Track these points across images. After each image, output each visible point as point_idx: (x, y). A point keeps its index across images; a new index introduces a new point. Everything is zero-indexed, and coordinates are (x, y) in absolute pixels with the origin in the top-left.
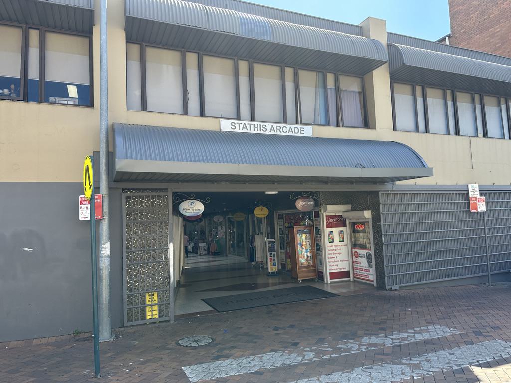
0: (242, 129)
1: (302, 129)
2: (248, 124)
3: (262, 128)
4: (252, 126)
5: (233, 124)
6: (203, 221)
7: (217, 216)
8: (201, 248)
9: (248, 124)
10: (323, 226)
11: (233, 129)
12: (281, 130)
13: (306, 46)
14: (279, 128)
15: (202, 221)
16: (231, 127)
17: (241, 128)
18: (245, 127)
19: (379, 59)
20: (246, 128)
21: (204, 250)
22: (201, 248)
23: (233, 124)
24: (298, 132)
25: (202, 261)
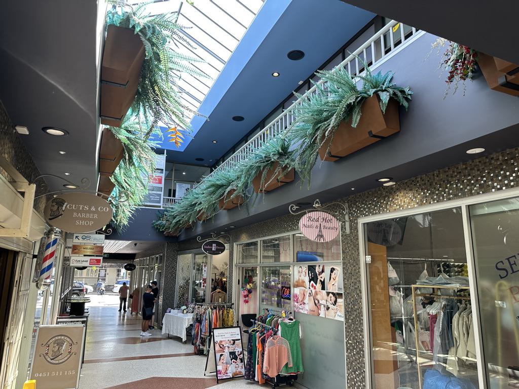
6: (226, 253)
7: (314, 215)
8: (222, 348)
15: (223, 251)
21: (233, 355)
22: (222, 348)
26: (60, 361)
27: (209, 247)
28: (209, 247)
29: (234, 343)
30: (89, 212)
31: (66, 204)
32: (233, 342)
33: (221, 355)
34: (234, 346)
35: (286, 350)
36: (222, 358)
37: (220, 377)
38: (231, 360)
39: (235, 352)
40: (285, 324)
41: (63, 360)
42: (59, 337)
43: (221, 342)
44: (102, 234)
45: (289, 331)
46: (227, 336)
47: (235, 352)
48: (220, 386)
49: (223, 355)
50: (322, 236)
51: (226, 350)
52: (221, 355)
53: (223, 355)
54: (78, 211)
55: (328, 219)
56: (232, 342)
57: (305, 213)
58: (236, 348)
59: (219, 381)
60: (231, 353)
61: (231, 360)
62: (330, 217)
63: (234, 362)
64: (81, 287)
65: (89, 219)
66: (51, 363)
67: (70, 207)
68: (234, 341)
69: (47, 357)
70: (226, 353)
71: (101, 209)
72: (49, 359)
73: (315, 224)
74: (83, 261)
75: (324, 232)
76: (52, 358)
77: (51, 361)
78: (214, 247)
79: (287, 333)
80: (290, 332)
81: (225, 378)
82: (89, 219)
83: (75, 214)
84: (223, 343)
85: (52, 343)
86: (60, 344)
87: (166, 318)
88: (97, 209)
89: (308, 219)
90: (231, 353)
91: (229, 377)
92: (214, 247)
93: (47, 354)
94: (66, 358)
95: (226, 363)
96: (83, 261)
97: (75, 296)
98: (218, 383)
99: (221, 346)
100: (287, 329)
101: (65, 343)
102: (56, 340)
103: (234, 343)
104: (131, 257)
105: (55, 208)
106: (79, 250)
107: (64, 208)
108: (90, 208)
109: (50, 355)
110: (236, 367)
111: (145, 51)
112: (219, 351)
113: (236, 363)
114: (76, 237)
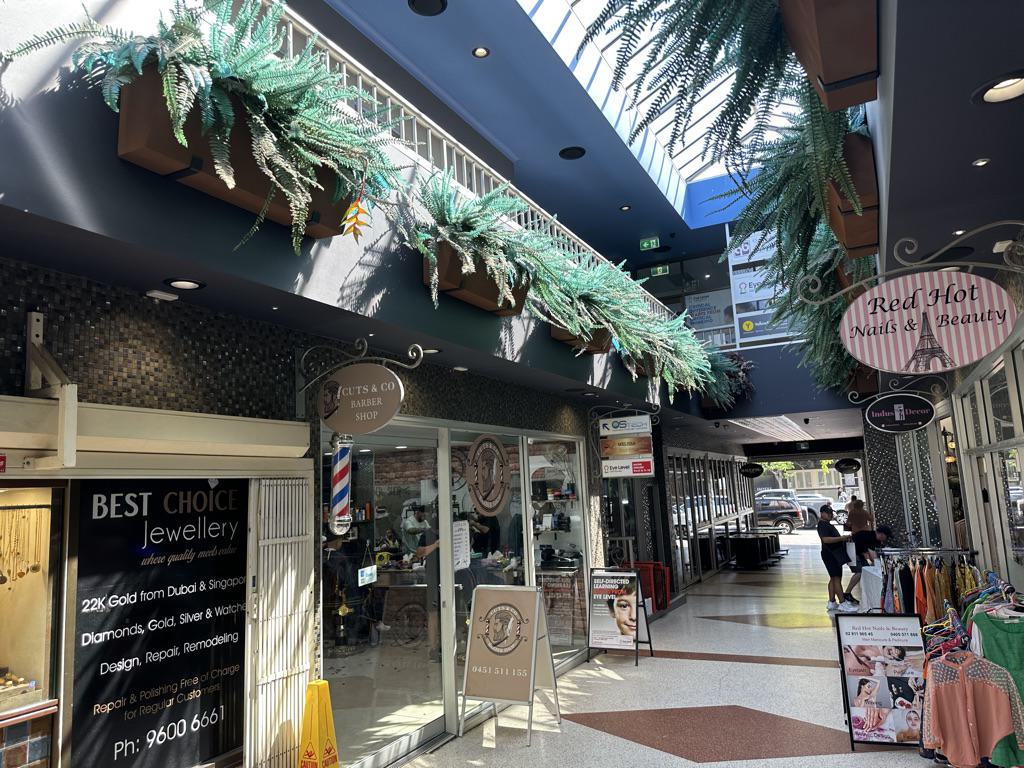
22: (866, 664)
26: (506, 650)
27: (883, 414)
28: (883, 414)
29: (902, 656)
30: (370, 395)
31: (340, 388)
32: (898, 652)
33: (863, 682)
34: (902, 663)
35: (1004, 699)
36: (865, 688)
37: (859, 734)
38: (895, 698)
39: (907, 679)
40: (996, 623)
41: (509, 649)
42: (503, 608)
43: (862, 648)
44: (645, 414)
45: (1010, 644)
46: (877, 634)
47: (907, 679)
48: (851, 759)
49: (867, 681)
50: (936, 352)
51: (878, 671)
52: (863, 682)
53: (867, 681)
54: (357, 397)
55: (956, 289)
56: (896, 653)
57: (861, 291)
58: (910, 670)
59: (855, 745)
60: (891, 680)
61: (895, 698)
62: (966, 280)
63: (902, 704)
64: (792, 508)
65: (371, 409)
66: (491, 650)
67: (346, 392)
68: (902, 652)
69: (487, 640)
70: (878, 678)
71: (385, 387)
72: (490, 645)
73: (900, 317)
74: (622, 468)
75: (942, 336)
76: (495, 642)
77: (495, 649)
78: (899, 412)
79: (1005, 646)
80: (1015, 645)
81: (875, 740)
82: (371, 409)
83: (353, 403)
84: (867, 652)
85: (493, 618)
86: (505, 621)
87: (865, 581)
88: (378, 388)
89: (870, 309)
90: (891, 680)
91: (887, 741)
92: (899, 412)
93: (487, 634)
94: (513, 646)
95: (879, 704)
96: (622, 468)
97: (785, 524)
98: (853, 749)
99: (863, 659)
100: (1000, 635)
101: (512, 619)
102: (498, 613)
103: (902, 656)
104: (853, 444)
105: (328, 399)
106: (612, 448)
107: (338, 396)
108: (370, 388)
109: (492, 635)
110: (910, 719)
111: (104, 98)
112: (856, 672)
113: (908, 706)
114: (604, 425)
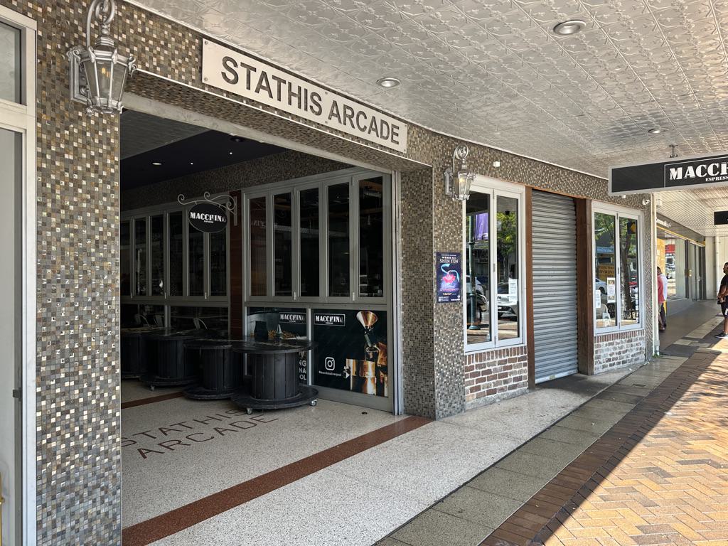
0: (257, 91)
1: (395, 130)
2: (274, 77)
3: (310, 103)
4: (284, 87)
5: (230, 64)
9: (274, 77)
10: (654, 237)
11: (228, 80)
12: (354, 120)
13: (538, 356)
14: (349, 113)
16: (224, 74)
17: (254, 84)
18: (264, 84)
19: (525, 365)
20: (268, 88)
23: (230, 64)
24: (387, 138)
25: (430, 361)
